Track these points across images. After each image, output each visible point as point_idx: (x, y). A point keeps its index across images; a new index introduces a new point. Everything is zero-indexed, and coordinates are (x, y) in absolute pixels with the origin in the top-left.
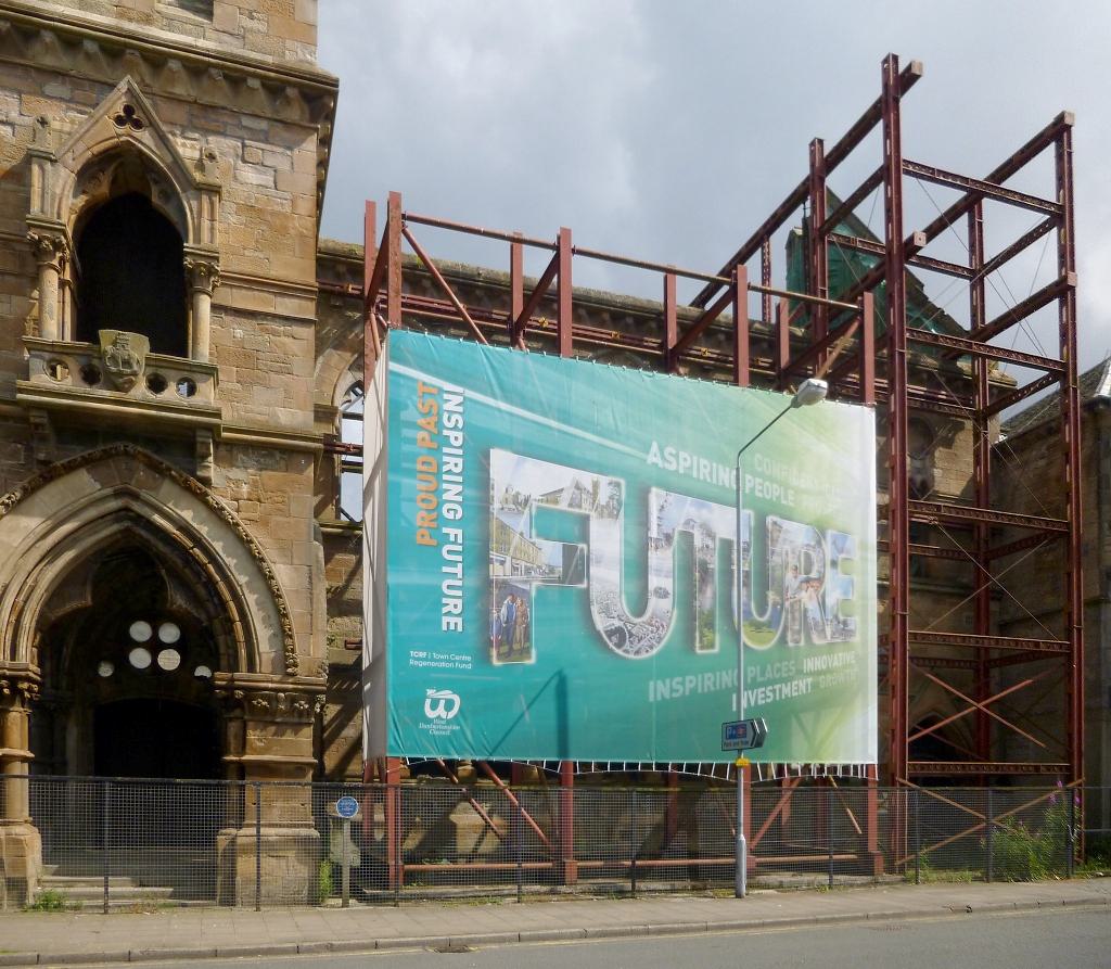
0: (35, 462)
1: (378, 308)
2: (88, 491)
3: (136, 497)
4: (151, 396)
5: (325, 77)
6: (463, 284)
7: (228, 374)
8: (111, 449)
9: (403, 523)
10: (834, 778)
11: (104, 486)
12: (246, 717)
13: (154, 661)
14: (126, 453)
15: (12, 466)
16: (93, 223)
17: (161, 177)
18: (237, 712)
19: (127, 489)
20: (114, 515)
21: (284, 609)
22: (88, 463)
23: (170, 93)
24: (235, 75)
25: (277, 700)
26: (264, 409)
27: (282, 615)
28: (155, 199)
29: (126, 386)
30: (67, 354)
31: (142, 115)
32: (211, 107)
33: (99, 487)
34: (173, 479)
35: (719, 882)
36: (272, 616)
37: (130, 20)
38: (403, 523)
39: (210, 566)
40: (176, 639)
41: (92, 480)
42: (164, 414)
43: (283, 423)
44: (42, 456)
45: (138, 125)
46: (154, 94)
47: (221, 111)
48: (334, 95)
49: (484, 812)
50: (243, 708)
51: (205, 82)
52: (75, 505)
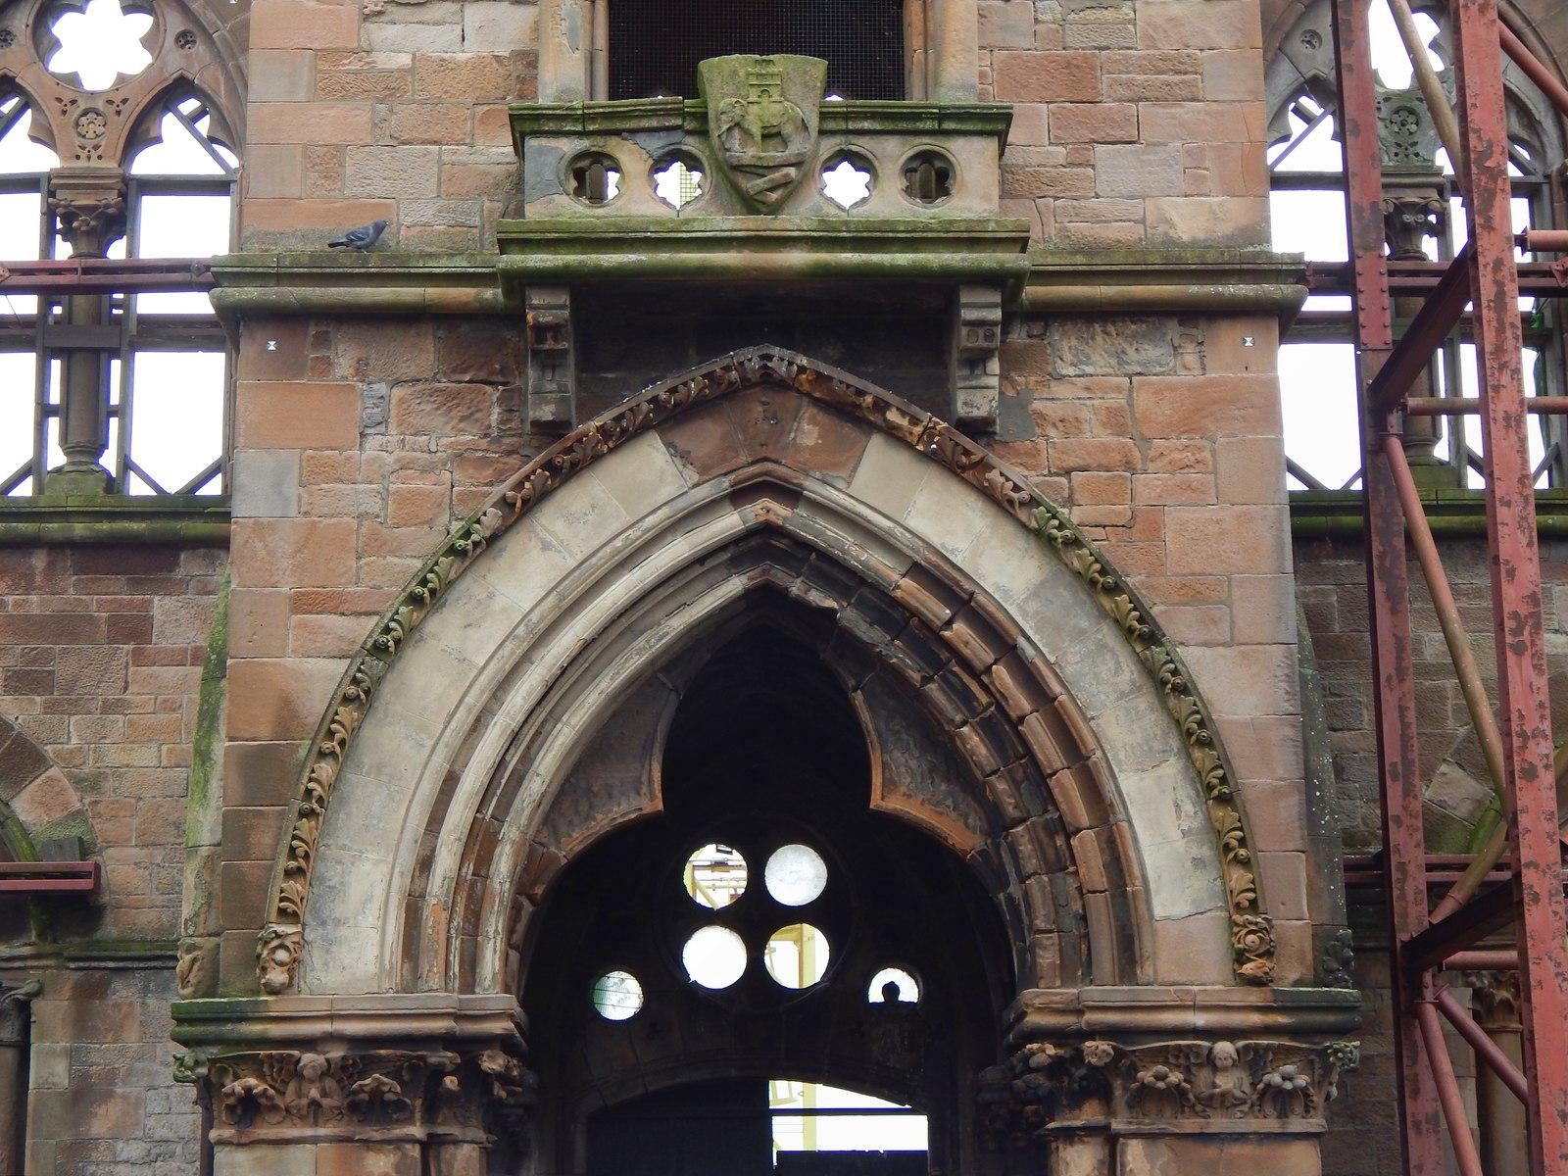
7: (1034, 137)
8: (727, 369)
10: (71, 777)
12: (1117, 1125)
13: (756, 965)
14: (768, 380)
18: (1090, 1114)
20: (732, 549)
21: (1175, 672)
22: (668, 419)
25: (1210, 1061)
26: (1135, 208)
29: (774, 196)
30: (617, 133)
33: (696, 478)
34: (893, 434)
35: (1133, 912)
36: (1188, 808)
38: (1358, 486)
49: (202, 164)
50: (1105, 1097)
52: (633, 534)
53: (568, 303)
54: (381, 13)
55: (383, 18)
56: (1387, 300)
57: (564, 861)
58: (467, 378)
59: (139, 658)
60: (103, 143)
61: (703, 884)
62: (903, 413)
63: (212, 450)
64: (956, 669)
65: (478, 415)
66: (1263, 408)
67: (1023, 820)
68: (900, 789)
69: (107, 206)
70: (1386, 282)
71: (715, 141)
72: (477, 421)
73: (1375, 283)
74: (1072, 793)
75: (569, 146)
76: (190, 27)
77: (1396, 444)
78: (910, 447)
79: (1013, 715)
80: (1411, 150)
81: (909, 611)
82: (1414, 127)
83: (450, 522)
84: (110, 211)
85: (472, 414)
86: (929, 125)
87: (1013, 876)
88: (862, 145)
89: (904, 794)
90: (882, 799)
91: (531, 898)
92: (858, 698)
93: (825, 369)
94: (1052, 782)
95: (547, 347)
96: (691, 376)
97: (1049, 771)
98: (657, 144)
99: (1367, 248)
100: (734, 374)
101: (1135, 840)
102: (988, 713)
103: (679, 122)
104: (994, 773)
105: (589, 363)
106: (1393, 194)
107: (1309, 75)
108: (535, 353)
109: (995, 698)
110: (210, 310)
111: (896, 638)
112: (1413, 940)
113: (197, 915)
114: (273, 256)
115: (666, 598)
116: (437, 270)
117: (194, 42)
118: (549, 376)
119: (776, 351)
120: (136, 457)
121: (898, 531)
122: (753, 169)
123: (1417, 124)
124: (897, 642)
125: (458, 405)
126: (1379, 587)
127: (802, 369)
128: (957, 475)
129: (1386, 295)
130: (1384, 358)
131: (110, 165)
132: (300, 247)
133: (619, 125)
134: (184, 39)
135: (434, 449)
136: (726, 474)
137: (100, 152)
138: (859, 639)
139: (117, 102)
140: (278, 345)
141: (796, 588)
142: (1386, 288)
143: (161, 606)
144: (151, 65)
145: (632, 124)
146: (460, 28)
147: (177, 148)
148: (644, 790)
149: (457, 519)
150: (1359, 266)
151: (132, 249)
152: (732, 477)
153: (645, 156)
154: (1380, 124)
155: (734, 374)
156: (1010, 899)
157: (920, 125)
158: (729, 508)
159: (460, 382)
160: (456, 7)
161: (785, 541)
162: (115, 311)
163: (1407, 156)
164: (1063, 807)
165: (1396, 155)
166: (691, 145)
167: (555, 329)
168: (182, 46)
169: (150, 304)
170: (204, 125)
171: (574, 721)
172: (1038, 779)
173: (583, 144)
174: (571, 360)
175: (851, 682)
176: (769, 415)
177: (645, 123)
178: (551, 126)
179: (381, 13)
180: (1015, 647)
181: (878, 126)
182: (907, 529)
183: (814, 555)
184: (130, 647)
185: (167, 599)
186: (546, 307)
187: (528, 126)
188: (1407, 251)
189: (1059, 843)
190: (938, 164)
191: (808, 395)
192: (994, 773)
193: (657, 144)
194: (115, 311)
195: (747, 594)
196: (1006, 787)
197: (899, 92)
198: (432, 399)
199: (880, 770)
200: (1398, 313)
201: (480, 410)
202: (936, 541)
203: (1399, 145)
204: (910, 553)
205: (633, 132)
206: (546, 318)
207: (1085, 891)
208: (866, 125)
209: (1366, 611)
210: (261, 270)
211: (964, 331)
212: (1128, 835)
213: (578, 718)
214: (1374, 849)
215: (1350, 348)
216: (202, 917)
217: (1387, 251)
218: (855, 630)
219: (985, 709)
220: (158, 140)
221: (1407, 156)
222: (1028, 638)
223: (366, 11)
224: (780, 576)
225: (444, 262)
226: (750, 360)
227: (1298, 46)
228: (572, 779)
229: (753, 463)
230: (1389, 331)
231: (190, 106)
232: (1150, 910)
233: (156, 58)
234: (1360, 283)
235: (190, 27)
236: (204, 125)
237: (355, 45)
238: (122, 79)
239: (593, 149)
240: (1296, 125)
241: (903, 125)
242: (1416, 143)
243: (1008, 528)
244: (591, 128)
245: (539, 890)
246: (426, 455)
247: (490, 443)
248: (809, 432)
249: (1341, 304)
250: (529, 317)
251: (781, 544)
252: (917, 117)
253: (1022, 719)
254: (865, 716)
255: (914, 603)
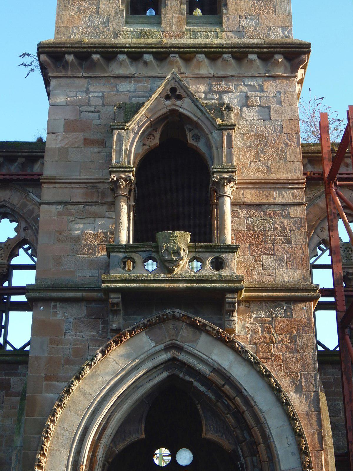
0: (109, 331)
1: (336, 185)
2: (146, 348)
3: (180, 349)
4: (216, 274)
5: (300, 44)
6: (310, 157)
8: (163, 315)
9: (338, 349)
11: (157, 344)
14: (174, 317)
15: (93, 336)
16: (147, 163)
17: (196, 125)
19: (175, 343)
22: (148, 327)
23: (197, 74)
24: (240, 54)
27: (298, 435)
28: (190, 141)
30: (135, 252)
31: (182, 91)
32: (224, 77)
33: (154, 345)
36: (290, 438)
37: (170, 37)
38: (338, 349)
39: (238, 399)
40: (192, 459)
41: (149, 340)
42: (203, 285)
43: (287, 280)
44: (115, 326)
45: (179, 97)
46: (187, 77)
47: (230, 78)
48: (308, 53)
49: (29, 261)
51: (219, 62)
53: (120, 297)
54: (73, 221)
55: (74, 222)
56: (344, 298)
57: (117, 452)
58: (93, 317)
59: (7, 395)
60: (3, 256)
61: (166, 460)
62: (211, 327)
63: (28, 338)
64: (225, 398)
65: (96, 327)
66: (310, 327)
67: (244, 441)
68: (210, 433)
69: (4, 272)
70: (344, 293)
71: (160, 254)
72: (95, 329)
73: (341, 294)
74: (258, 434)
75: (121, 255)
76: (27, 226)
77: (347, 337)
78: (212, 336)
79: (241, 411)
80: (350, 258)
81: (212, 382)
82: (351, 252)
83: (88, 356)
84: (4, 274)
85: (94, 327)
86: (217, 250)
87: (242, 458)
88: (199, 255)
89: (211, 434)
90: (205, 435)
91: (108, 462)
92: (199, 406)
93: (190, 315)
94: (252, 430)
95: (115, 309)
96: (153, 317)
97: (251, 427)
98: (145, 255)
99: (338, 284)
100: (165, 316)
101: (275, 447)
102: (234, 411)
103: (151, 249)
104: (236, 427)
105: (126, 314)
106: (346, 270)
107: (322, 239)
108: (112, 310)
109: (236, 406)
110: (26, 300)
111: (209, 389)
112: (168, 465)
113: (16, 466)
114: (43, 284)
115: (146, 378)
116: (86, 288)
117: (28, 230)
118: (115, 317)
119: (176, 310)
120: (9, 339)
121: (209, 360)
122: (170, 262)
123: (352, 251)
124: (209, 391)
125: (91, 325)
126: (344, 377)
127: (183, 315)
128: (225, 344)
129: (344, 297)
130: (344, 314)
131: (5, 261)
132: (50, 282)
133: (135, 250)
134: (25, 229)
135: (84, 336)
136: (162, 344)
137: (2, 258)
138: (199, 390)
139: (7, 245)
140: (43, 308)
141: (181, 375)
142: (344, 295)
143: (13, 379)
144: (16, 236)
145: (139, 250)
146: (94, 224)
147: (23, 258)
148: (139, 432)
149: (90, 356)
150: (336, 289)
151: (10, 283)
152: (164, 344)
153: (142, 258)
154: (342, 252)
155: (165, 316)
156: (241, 464)
157: (215, 250)
158: (163, 352)
159: (92, 318)
160: (93, 219)
161: (178, 362)
162: (5, 300)
163: (349, 260)
164: (255, 437)
165: (346, 260)
166: (154, 255)
167: (117, 304)
168: (25, 231)
169: (14, 298)
170: (30, 251)
171: (120, 412)
172: (248, 429)
173: (126, 255)
174: (122, 312)
175: (197, 402)
176: (175, 328)
177: (142, 249)
178: (117, 250)
179: (73, 221)
180: (242, 392)
181: (204, 250)
182: (212, 359)
183: (186, 366)
184: (4, 391)
185: (15, 378)
186: (115, 298)
187: (111, 250)
188: (350, 285)
189: (254, 448)
190: (220, 260)
191: (185, 322)
192: (236, 427)
193: (145, 255)
194: (5, 300)
195: (168, 377)
196: (239, 432)
197: (210, 240)
198: (84, 323)
199: (205, 427)
200: (347, 302)
201: (96, 326)
202: (219, 362)
203: (347, 257)
204: (212, 365)
205: (139, 251)
206: (115, 301)
207: (262, 461)
208: (201, 250)
209: (341, 384)
210: (39, 288)
211: (227, 305)
212: (273, 445)
213: (121, 411)
214: (346, 451)
215: (335, 311)
216: (17, 467)
217: (344, 285)
218: (198, 387)
219: (234, 409)
220: (18, 255)
221: (349, 260)
222: (245, 390)
223: (70, 220)
224: (176, 372)
225: (88, 286)
226: (169, 313)
227: (319, 231)
228: (120, 429)
229: (170, 341)
230: (345, 307)
231: (26, 246)
232: (280, 467)
233: (18, 234)
234: (337, 294)
235: (27, 226)
236: (30, 251)
237: (67, 229)
238: (9, 239)
239: (128, 256)
240: (319, 252)
241: (211, 250)
242: (351, 257)
243: (240, 359)
244: (128, 251)
245: (110, 460)
246: (82, 338)
247: (99, 335)
248: (185, 332)
249: (332, 299)
250: (110, 301)
251: (178, 363)
252: (214, 248)
253: (244, 412)
254: (201, 411)
255: (214, 380)
